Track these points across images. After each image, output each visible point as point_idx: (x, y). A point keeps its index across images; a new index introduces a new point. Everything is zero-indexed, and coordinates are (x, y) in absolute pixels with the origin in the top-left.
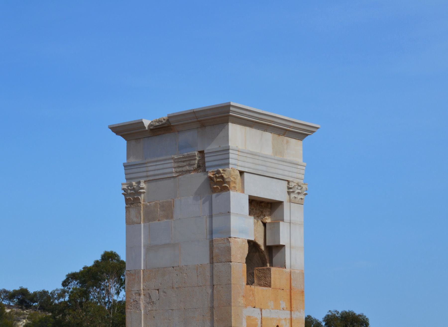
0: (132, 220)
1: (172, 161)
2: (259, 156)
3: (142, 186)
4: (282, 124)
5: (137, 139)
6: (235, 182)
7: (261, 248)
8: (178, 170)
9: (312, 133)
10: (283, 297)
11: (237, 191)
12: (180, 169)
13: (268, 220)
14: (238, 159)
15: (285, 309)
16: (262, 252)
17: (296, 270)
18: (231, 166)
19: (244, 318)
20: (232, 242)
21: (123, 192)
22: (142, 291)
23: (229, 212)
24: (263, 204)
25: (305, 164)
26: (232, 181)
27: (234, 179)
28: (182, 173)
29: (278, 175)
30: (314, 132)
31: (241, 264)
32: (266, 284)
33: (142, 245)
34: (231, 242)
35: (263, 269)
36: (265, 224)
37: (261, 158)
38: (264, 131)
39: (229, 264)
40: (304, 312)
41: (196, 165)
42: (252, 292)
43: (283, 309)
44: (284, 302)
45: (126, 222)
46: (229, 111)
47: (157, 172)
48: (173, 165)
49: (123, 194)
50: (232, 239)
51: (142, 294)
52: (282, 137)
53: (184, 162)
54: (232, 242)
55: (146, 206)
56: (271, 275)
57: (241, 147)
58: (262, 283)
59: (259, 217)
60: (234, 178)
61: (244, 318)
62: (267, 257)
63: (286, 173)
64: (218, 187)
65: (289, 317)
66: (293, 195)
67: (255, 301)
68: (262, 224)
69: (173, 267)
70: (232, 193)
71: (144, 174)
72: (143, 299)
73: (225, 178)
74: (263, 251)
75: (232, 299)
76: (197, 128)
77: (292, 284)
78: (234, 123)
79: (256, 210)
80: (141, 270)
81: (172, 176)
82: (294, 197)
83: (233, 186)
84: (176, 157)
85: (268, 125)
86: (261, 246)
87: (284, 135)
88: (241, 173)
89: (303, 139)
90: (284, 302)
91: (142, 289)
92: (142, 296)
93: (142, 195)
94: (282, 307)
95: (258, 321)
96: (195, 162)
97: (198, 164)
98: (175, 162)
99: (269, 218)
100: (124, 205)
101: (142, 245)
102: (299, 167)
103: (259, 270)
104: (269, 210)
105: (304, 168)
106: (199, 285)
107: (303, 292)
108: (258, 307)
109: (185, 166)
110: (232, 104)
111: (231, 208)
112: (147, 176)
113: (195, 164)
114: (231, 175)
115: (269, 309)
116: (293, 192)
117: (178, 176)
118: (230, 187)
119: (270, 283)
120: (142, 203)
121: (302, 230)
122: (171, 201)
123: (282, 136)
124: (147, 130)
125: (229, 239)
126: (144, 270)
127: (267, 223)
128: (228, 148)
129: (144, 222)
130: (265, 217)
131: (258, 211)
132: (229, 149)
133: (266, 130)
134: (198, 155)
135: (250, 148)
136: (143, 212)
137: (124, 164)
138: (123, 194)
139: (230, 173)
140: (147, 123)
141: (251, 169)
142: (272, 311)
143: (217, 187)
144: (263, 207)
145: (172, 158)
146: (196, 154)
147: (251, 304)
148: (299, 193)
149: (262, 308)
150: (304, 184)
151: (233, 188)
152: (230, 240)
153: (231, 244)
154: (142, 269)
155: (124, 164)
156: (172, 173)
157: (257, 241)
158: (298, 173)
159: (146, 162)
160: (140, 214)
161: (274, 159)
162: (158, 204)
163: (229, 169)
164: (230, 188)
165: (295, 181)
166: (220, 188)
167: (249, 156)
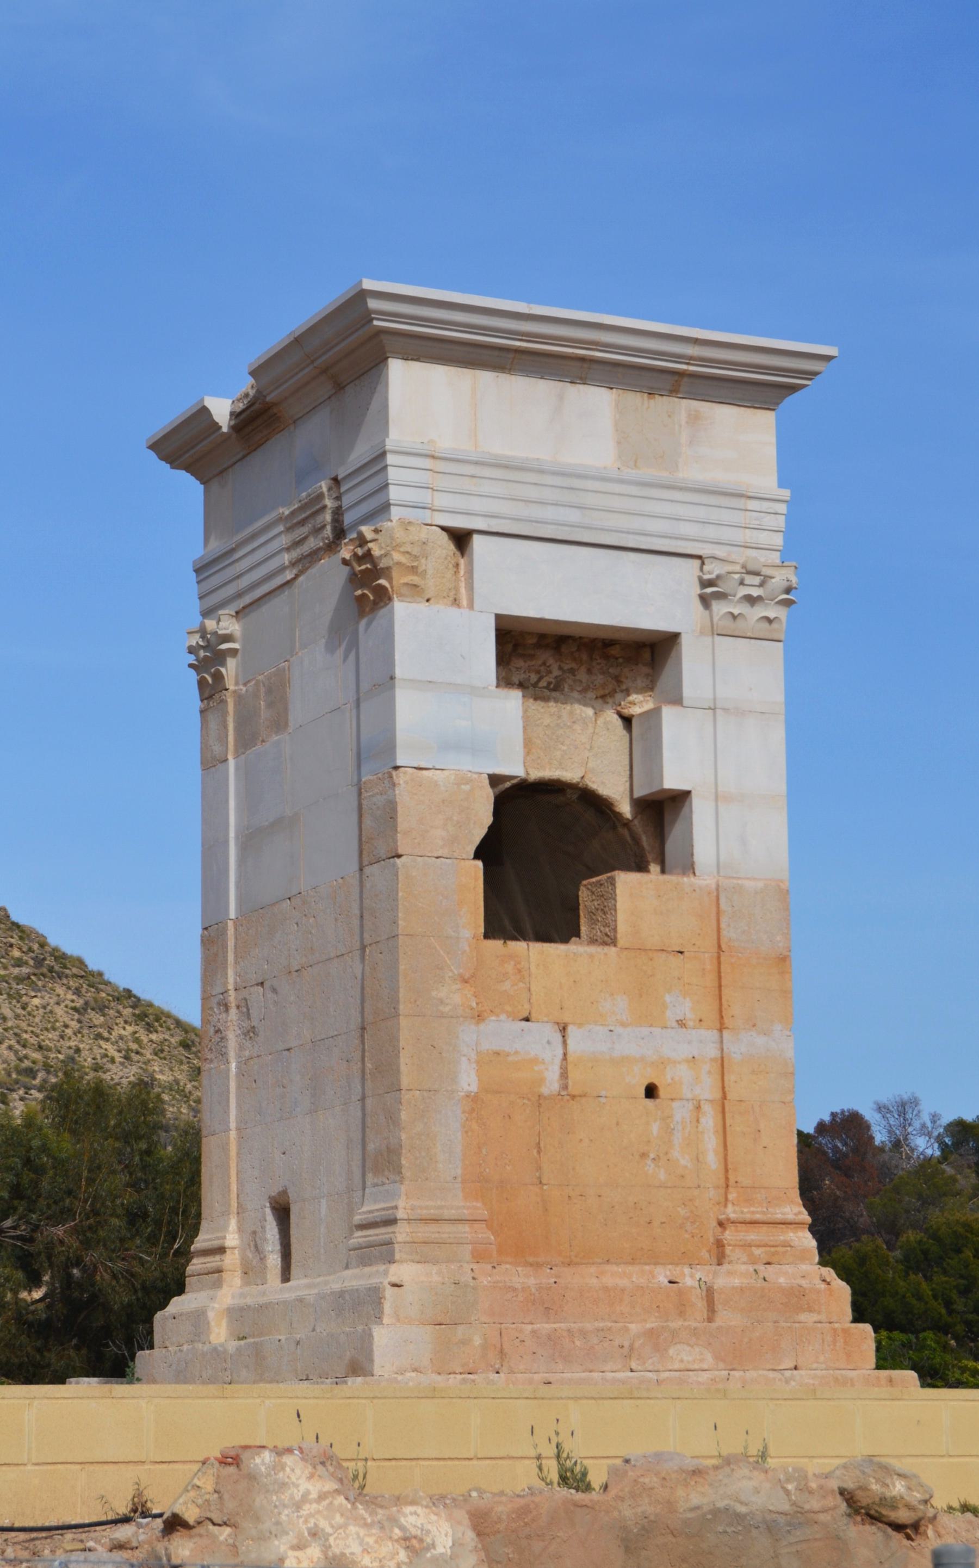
1: (281, 528)
2: (542, 472)
3: (225, 629)
4: (606, 347)
5: (221, 472)
7: (617, 810)
8: (295, 554)
9: (811, 379)
10: (679, 979)
11: (428, 600)
13: (639, 704)
14: (431, 486)
15: (691, 1024)
16: (627, 824)
17: (748, 879)
18: (395, 512)
19: (464, 1059)
20: (401, 782)
21: (191, 659)
22: (232, 993)
23: (392, 678)
24: (614, 651)
25: (786, 494)
26: (398, 563)
27: (408, 556)
29: (680, 543)
30: (816, 374)
31: (448, 861)
32: (606, 935)
33: (232, 834)
34: (399, 784)
35: (600, 881)
36: (627, 721)
37: (548, 480)
38: (571, 382)
39: (394, 865)
40: (788, 1033)
41: (329, 528)
42: (512, 963)
43: (681, 1024)
44: (684, 998)
46: (368, 317)
48: (285, 540)
49: (191, 666)
50: (405, 773)
51: (233, 1005)
52: (662, 404)
54: (403, 785)
55: (239, 698)
56: (616, 901)
57: (446, 443)
58: (599, 933)
59: (610, 700)
60: (408, 552)
61: (464, 1059)
62: (645, 841)
64: (366, 592)
65: (713, 1052)
66: (719, 608)
67: (531, 994)
68: (618, 722)
69: (289, 899)
70: (401, 609)
71: (230, 590)
72: (235, 1023)
73: (378, 558)
74: (628, 819)
75: (401, 990)
76: (329, 398)
77: (724, 933)
78: (412, 359)
79: (589, 671)
80: (226, 924)
81: (285, 581)
82: (730, 617)
83: (406, 584)
84: (287, 513)
85: (582, 359)
86: (616, 804)
87: (674, 391)
89: (778, 404)
90: (684, 998)
91: (231, 987)
92: (233, 1011)
93: (231, 663)
94: (671, 1016)
95: (547, 1069)
96: (324, 518)
97: (337, 525)
98: (289, 530)
99: (649, 698)
100: (197, 704)
101: (232, 834)
102: (752, 504)
103: (589, 887)
104: (646, 670)
105: (782, 508)
107: (783, 960)
108: (546, 1019)
109: (305, 538)
110: (368, 284)
111: (397, 662)
112: (239, 595)
113: (324, 527)
114: (394, 544)
115: (608, 1025)
116: (721, 596)
117: (297, 576)
118: (392, 587)
120: (231, 686)
121: (778, 736)
123: (665, 397)
124: (226, 437)
125: (394, 773)
126: (236, 922)
127: (633, 716)
128: (381, 451)
129: (237, 756)
130: (629, 695)
131: (602, 677)
132: (383, 454)
133: (581, 378)
134: (332, 492)
135: (497, 447)
136: (234, 722)
138: (191, 666)
139: (392, 538)
141: (503, 521)
142: (619, 1030)
143: (364, 595)
144: (621, 660)
145: (280, 519)
146: (325, 489)
147: (508, 1008)
148: (751, 600)
149: (566, 1020)
150: (780, 564)
151: (405, 590)
152: (395, 777)
153: (397, 792)
154: (232, 915)
156: (282, 569)
157: (593, 786)
158: (751, 526)
159: (234, 546)
160: (225, 727)
161: (622, 481)
162: (261, 685)
163: (389, 523)
164: (393, 591)
165: (733, 557)
166: (372, 598)
167: (487, 472)
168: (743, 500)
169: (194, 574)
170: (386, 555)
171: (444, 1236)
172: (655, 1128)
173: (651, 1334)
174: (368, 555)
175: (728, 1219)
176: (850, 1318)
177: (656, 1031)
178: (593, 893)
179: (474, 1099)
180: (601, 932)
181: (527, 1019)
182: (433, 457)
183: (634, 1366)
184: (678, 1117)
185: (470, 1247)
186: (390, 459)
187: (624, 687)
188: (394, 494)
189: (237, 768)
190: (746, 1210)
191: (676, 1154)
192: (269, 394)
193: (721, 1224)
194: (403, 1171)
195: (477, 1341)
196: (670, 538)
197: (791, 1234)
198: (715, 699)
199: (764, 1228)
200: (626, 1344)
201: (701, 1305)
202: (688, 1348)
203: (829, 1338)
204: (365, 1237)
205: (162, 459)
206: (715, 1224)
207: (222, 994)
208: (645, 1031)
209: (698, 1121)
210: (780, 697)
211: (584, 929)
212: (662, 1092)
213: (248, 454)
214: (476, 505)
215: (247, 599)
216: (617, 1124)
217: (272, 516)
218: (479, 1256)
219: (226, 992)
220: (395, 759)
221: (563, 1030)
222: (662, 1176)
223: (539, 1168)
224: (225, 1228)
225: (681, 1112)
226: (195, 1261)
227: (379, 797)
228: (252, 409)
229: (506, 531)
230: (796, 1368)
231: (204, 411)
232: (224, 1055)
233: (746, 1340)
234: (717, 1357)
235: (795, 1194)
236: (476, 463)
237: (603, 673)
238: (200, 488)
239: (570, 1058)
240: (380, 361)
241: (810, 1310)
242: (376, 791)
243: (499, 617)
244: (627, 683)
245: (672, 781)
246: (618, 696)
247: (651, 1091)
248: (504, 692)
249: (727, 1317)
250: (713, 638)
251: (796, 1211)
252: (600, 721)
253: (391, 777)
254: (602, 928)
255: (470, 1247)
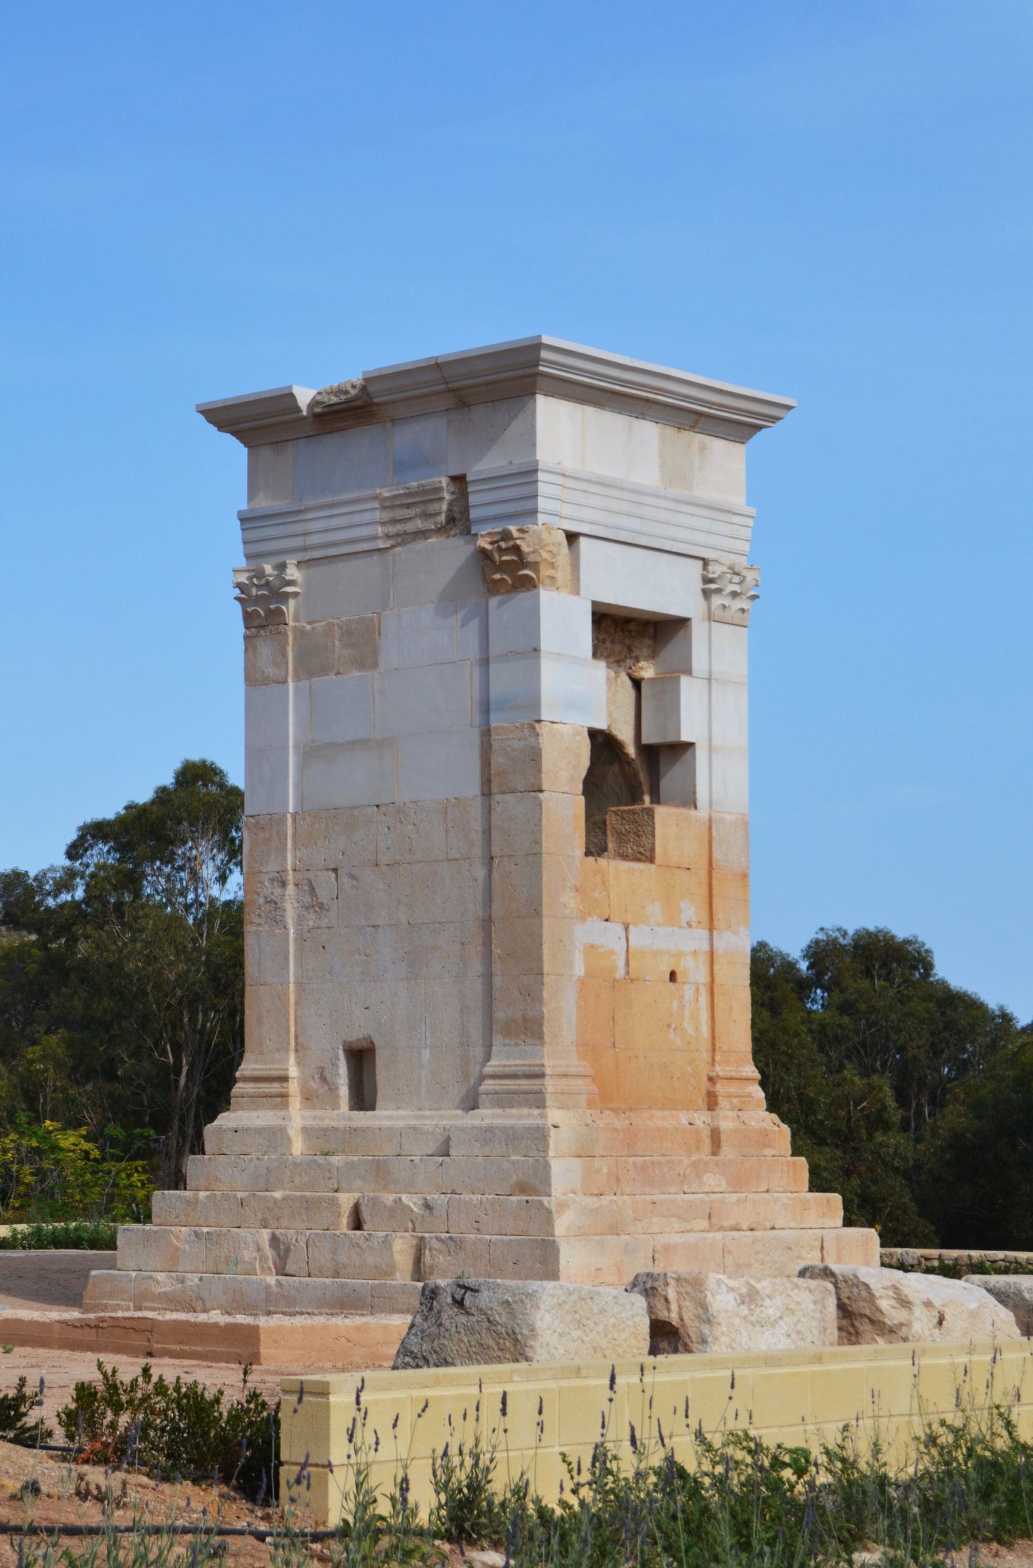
0: (263, 672)
1: (376, 505)
2: (622, 489)
6: (553, 563)
8: (393, 529)
9: (774, 422)
12: (393, 529)
13: (647, 671)
15: (694, 924)
16: (629, 761)
18: (541, 518)
21: (237, 592)
23: (536, 650)
24: (632, 627)
25: (752, 511)
26: (545, 560)
28: (404, 538)
30: (779, 419)
33: (291, 744)
35: (633, 810)
36: (637, 683)
37: (627, 496)
38: (636, 417)
41: (443, 515)
43: (689, 925)
45: (247, 678)
46: (537, 362)
47: (331, 537)
48: (377, 515)
49: (236, 598)
50: (545, 726)
52: (687, 436)
53: (408, 506)
55: (300, 633)
56: (654, 828)
57: (570, 465)
58: (630, 851)
59: (622, 664)
60: (550, 551)
61: (577, 951)
62: (643, 777)
63: (699, 537)
64: (505, 577)
66: (717, 601)
69: (378, 806)
71: (297, 542)
74: (632, 759)
78: (550, 396)
79: (612, 642)
81: (376, 547)
84: (386, 494)
85: (647, 400)
87: (692, 428)
88: (572, 537)
89: (748, 439)
91: (289, 867)
93: (292, 603)
96: (441, 507)
98: (384, 508)
101: (291, 744)
102: (735, 519)
105: (750, 522)
106: (450, 857)
107: (745, 876)
110: (546, 340)
112: (305, 549)
116: (719, 591)
117: (393, 547)
118: (538, 578)
119: (653, 850)
121: (744, 700)
122: (372, 620)
124: (304, 418)
125: (537, 725)
126: (295, 816)
127: (643, 679)
133: (642, 414)
136: (293, 651)
137: (239, 513)
138: (236, 598)
140: (304, 396)
142: (656, 929)
143: (502, 580)
144: (633, 634)
145: (376, 498)
146: (444, 485)
151: (547, 581)
153: (541, 741)
155: (239, 513)
156: (374, 538)
159: (303, 508)
161: (665, 498)
163: (536, 527)
164: (539, 581)
166: (510, 582)
167: (593, 488)
168: (730, 515)
169: (238, 522)
170: (534, 552)
171: (572, 1088)
172: (675, 1004)
173: (694, 1165)
174: (516, 549)
175: (718, 1076)
176: (790, 1152)
177: (676, 929)
178: (623, 818)
179: (581, 982)
180: (633, 850)
181: (607, 920)
182: (564, 475)
183: (686, 1189)
184: (686, 998)
185: (585, 1096)
186: (541, 476)
187: (634, 655)
188: (542, 504)
189: (297, 690)
190: (726, 1069)
191: (686, 1025)
192: (376, 397)
193: (711, 1079)
194: (545, 1037)
195: (605, 1170)
196: (689, 543)
197: (751, 1088)
198: (710, 672)
199: (736, 1083)
200: (682, 1173)
201: (707, 1141)
202: (713, 1176)
203: (786, 1169)
204: (501, 1085)
205: (210, 422)
206: (705, 1079)
207: (278, 872)
208: (670, 929)
209: (697, 1000)
210: (745, 672)
211: (611, 846)
212: (679, 977)
213: (317, 435)
214: (585, 514)
215: (309, 555)
216: (655, 1002)
217: (366, 493)
218: (590, 1104)
219: (283, 871)
220: (539, 714)
221: (627, 929)
222: (679, 1042)
223: (614, 1036)
224: (288, 1060)
225: (689, 992)
226: (237, 1085)
227: (516, 742)
228: (350, 404)
229: (629, 541)
230: (768, 1191)
231: (291, 396)
232: (279, 920)
233: (743, 1169)
234: (729, 1183)
235: (750, 1057)
236: (587, 481)
237: (620, 643)
238: (245, 451)
239: (630, 951)
240: (531, 393)
241: (770, 1146)
242: (511, 736)
243: (595, 604)
244: (636, 652)
245: (685, 737)
246: (629, 662)
247: (673, 976)
248: (596, 662)
249: (727, 1152)
250: (710, 624)
251: (751, 1070)
252: (619, 681)
253: (534, 728)
254: (635, 848)
255: (585, 1096)
